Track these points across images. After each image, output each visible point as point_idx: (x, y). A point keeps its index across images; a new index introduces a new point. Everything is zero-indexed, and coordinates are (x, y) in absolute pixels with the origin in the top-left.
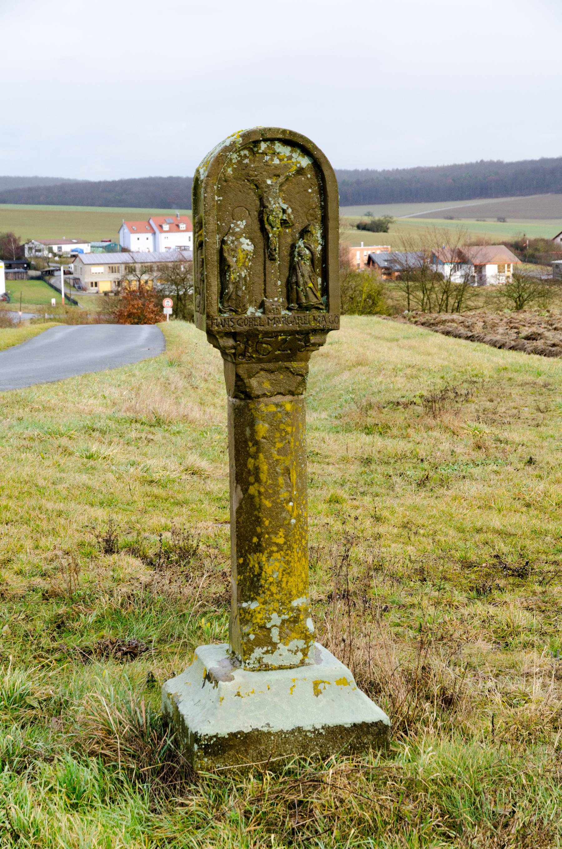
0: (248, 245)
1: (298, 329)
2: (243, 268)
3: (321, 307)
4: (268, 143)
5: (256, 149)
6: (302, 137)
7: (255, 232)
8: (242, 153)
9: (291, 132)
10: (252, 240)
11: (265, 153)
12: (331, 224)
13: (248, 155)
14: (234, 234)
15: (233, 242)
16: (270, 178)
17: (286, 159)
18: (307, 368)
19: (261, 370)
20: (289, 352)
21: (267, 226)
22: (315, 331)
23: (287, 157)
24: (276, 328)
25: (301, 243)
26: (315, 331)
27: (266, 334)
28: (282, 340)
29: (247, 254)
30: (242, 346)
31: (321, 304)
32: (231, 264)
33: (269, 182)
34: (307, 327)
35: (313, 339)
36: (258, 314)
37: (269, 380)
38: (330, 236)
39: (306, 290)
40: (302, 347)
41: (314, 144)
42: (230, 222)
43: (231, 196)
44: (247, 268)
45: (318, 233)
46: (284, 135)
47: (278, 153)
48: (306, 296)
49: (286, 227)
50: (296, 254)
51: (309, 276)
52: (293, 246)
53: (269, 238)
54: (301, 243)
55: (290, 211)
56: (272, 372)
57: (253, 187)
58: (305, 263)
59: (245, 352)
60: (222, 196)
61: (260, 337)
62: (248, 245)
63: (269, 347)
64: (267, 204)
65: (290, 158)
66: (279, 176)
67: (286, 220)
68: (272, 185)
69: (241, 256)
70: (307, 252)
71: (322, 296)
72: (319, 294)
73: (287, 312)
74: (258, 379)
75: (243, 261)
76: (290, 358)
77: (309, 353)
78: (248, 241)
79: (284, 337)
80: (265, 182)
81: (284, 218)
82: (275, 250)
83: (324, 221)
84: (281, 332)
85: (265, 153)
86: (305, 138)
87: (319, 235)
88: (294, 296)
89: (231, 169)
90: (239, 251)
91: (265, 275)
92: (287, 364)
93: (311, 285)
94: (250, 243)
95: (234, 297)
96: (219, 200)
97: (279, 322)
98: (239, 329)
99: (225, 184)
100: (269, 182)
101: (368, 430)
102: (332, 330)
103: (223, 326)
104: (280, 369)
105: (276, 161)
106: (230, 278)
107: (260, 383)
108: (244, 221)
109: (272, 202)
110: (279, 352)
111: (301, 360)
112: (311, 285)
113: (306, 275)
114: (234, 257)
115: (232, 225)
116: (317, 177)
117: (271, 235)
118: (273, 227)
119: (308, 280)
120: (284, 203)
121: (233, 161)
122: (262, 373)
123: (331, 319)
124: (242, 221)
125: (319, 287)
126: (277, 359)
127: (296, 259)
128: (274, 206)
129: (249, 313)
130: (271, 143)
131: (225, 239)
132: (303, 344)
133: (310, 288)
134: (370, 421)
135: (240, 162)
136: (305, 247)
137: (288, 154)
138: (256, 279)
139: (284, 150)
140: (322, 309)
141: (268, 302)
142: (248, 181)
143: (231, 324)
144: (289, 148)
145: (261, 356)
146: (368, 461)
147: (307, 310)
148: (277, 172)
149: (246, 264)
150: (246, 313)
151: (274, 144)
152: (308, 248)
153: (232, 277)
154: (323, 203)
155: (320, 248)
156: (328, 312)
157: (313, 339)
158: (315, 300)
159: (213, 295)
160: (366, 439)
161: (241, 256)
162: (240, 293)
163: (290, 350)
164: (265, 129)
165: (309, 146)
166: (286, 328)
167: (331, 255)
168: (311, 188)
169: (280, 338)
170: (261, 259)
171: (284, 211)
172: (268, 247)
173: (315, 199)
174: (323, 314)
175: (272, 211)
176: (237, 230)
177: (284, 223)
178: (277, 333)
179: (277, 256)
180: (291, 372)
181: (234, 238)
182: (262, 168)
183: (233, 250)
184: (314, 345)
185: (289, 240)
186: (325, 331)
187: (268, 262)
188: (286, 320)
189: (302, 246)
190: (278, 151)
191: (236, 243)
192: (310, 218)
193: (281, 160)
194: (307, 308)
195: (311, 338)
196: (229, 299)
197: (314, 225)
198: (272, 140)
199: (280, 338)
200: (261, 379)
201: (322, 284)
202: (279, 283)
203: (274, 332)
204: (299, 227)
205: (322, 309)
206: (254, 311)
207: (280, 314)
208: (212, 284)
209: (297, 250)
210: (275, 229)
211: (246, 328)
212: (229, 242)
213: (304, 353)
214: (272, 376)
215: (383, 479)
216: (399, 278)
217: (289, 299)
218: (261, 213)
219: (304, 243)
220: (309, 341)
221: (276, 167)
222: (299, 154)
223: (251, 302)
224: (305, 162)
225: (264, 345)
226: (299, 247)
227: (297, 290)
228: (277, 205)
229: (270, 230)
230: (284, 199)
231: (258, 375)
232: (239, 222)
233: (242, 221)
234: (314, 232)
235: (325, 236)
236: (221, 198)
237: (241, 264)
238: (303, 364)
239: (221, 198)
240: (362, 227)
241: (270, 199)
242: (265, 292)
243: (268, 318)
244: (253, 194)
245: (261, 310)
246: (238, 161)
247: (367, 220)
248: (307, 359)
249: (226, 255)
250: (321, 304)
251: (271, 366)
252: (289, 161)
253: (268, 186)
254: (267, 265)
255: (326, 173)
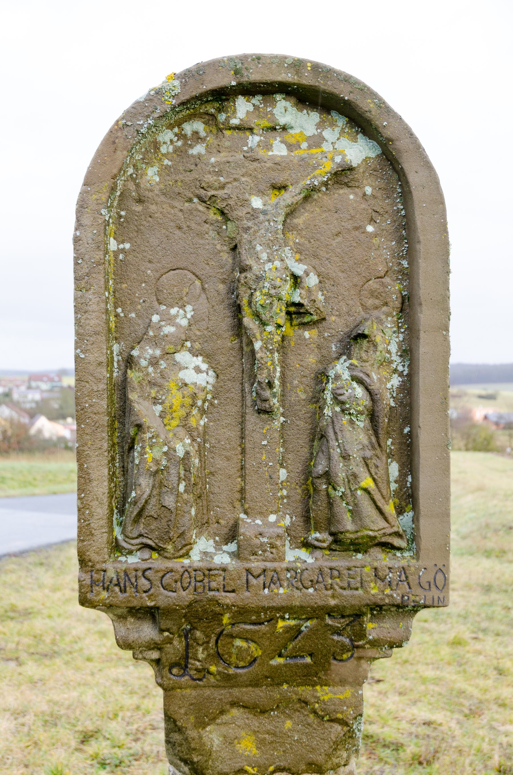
0: (198, 370)
1: (333, 602)
2: (182, 432)
3: (397, 542)
4: (257, 100)
5: (222, 117)
6: (347, 79)
7: (219, 336)
8: (188, 128)
9: (316, 68)
10: (208, 357)
11: (244, 128)
12: (425, 317)
13: (203, 134)
14: (155, 342)
15: (154, 362)
16: (261, 193)
17: (304, 145)
18: (358, 704)
19: (234, 704)
20: (308, 660)
21: (248, 321)
22: (378, 609)
23: (308, 139)
24: (270, 598)
25: (341, 368)
26: (378, 609)
27: (242, 613)
28: (288, 629)
29: (194, 396)
30: (178, 644)
31: (397, 534)
32: (146, 421)
33: (257, 203)
34: (356, 597)
35: (373, 629)
36: (222, 559)
37: (255, 732)
38: (425, 349)
39: (353, 495)
40: (344, 649)
41: (380, 99)
42: (151, 310)
43: (154, 241)
44: (190, 431)
45: (388, 340)
46: (297, 73)
47: (284, 128)
48: (356, 513)
49: (304, 325)
50: (328, 396)
51: (365, 459)
52: (321, 377)
53: (253, 352)
54: (341, 368)
55: (312, 280)
56: (263, 712)
57: (213, 216)
58: (351, 422)
59: (187, 657)
60: (130, 240)
61: (226, 619)
62: (198, 370)
63: (253, 646)
64: (250, 262)
65: (316, 141)
66: (284, 187)
67: (300, 305)
68: (264, 213)
69: (176, 398)
70: (359, 391)
71: (400, 511)
72: (390, 509)
73: (303, 554)
74: (224, 729)
75: (182, 412)
76: (311, 676)
77: (364, 664)
78: (199, 361)
79: (292, 623)
80: (246, 202)
81: (297, 299)
82: (270, 385)
83: (407, 307)
84: (283, 609)
85: (244, 128)
86: (357, 82)
87: (393, 348)
88: (319, 509)
89: (155, 169)
90: (172, 385)
91: (243, 452)
92: (305, 691)
93: (368, 482)
94: (204, 367)
95: (152, 510)
96: (123, 251)
97: (276, 580)
98: (164, 598)
99: (138, 208)
100: (257, 203)
101: (488, 554)
102: (425, 607)
103: (123, 591)
104: (282, 705)
105: (279, 150)
106: (143, 461)
107: (230, 742)
108: (189, 308)
109: (264, 256)
110: (281, 661)
111: (343, 682)
112: (368, 482)
113: (355, 454)
114: (155, 401)
115: (155, 318)
116: (388, 191)
117: (258, 345)
118: (263, 324)
119: (361, 471)
120: (300, 261)
121: (163, 149)
122: (235, 712)
123: (426, 577)
124: (183, 307)
125: (394, 486)
126: (275, 678)
127: (327, 412)
128: (268, 266)
129: (195, 556)
130: (265, 101)
131: (135, 353)
132: (347, 641)
133: (366, 490)
134: (489, 545)
135: (180, 153)
136: (354, 378)
137: (311, 130)
138: (220, 463)
139: (304, 122)
140: (399, 549)
141: (250, 525)
142: (202, 200)
143: (143, 583)
144: (315, 117)
145: (232, 671)
146: (488, 589)
147: (357, 551)
148: (280, 179)
149: (192, 422)
150: (187, 555)
151: (274, 103)
152: (360, 382)
153: (149, 456)
154: (405, 263)
155: (396, 381)
156: (417, 556)
157: (373, 629)
158: (382, 524)
159: (95, 503)
160: (486, 563)
161: (176, 398)
162: (169, 501)
163: (311, 655)
164: (243, 58)
165: (366, 105)
166: (297, 598)
167: (424, 402)
168: (372, 221)
169: (281, 624)
170: (234, 409)
171: (296, 280)
172: (253, 377)
173: (383, 252)
174: (403, 563)
175: (259, 279)
176: (169, 330)
177: (296, 312)
178: (272, 613)
179: (275, 402)
180: (315, 712)
181: (158, 352)
182: (238, 165)
183: (152, 384)
184: (375, 644)
185: (312, 360)
186: (406, 609)
187: (252, 418)
188: (298, 577)
189: (346, 375)
190: (282, 120)
191: (163, 364)
192: (370, 302)
193: (290, 147)
194: (358, 546)
195: (370, 626)
196: (140, 514)
197: (380, 321)
198: (266, 90)
199: (281, 624)
200: (230, 731)
201: (401, 480)
202: (283, 474)
203: (265, 609)
204: (338, 324)
205: (399, 549)
206: (211, 550)
207: (282, 559)
208: (93, 476)
209: (330, 386)
210: (269, 328)
211: (186, 596)
212: (144, 363)
213: (351, 664)
214: (265, 723)
215: (503, 612)
216: (505, 428)
217: (307, 519)
218: (233, 289)
219: (351, 367)
220: (361, 634)
221: (278, 164)
222: (342, 132)
223: (203, 525)
224: (357, 151)
225: (239, 643)
226: (337, 377)
227: (328, 495)
228: (277, 263)
229: (258, 335)
230: (298, 250)
231: (225, 718)
232: (174, 311)
233: (183, 307)
234: (378, 339)
235: (408, 352)
236: (127, 246)
237: (175, 423)
238: (346, 693)
239: (127, 246)
240: (481, 397)
241: (259, 248)
242: (243, 499)
243: (248, 571)
244: (213, 234)
245: (232, 547)
246: (175, 151)
247: (483, 393)
248: (358, 682)
249: (133, 396)
250: (397, 534)
251: (259, 695)
252: (314, 151)
253: (254, 214)
254: (249, 426)
255: (415, 178)
